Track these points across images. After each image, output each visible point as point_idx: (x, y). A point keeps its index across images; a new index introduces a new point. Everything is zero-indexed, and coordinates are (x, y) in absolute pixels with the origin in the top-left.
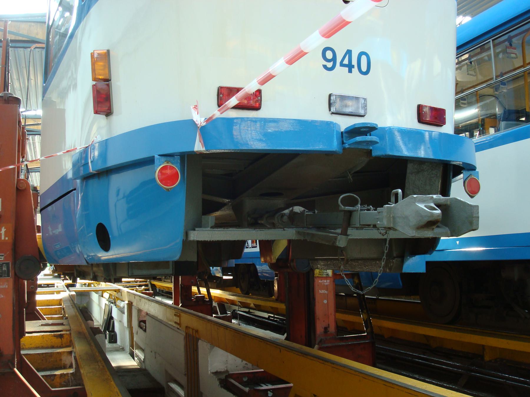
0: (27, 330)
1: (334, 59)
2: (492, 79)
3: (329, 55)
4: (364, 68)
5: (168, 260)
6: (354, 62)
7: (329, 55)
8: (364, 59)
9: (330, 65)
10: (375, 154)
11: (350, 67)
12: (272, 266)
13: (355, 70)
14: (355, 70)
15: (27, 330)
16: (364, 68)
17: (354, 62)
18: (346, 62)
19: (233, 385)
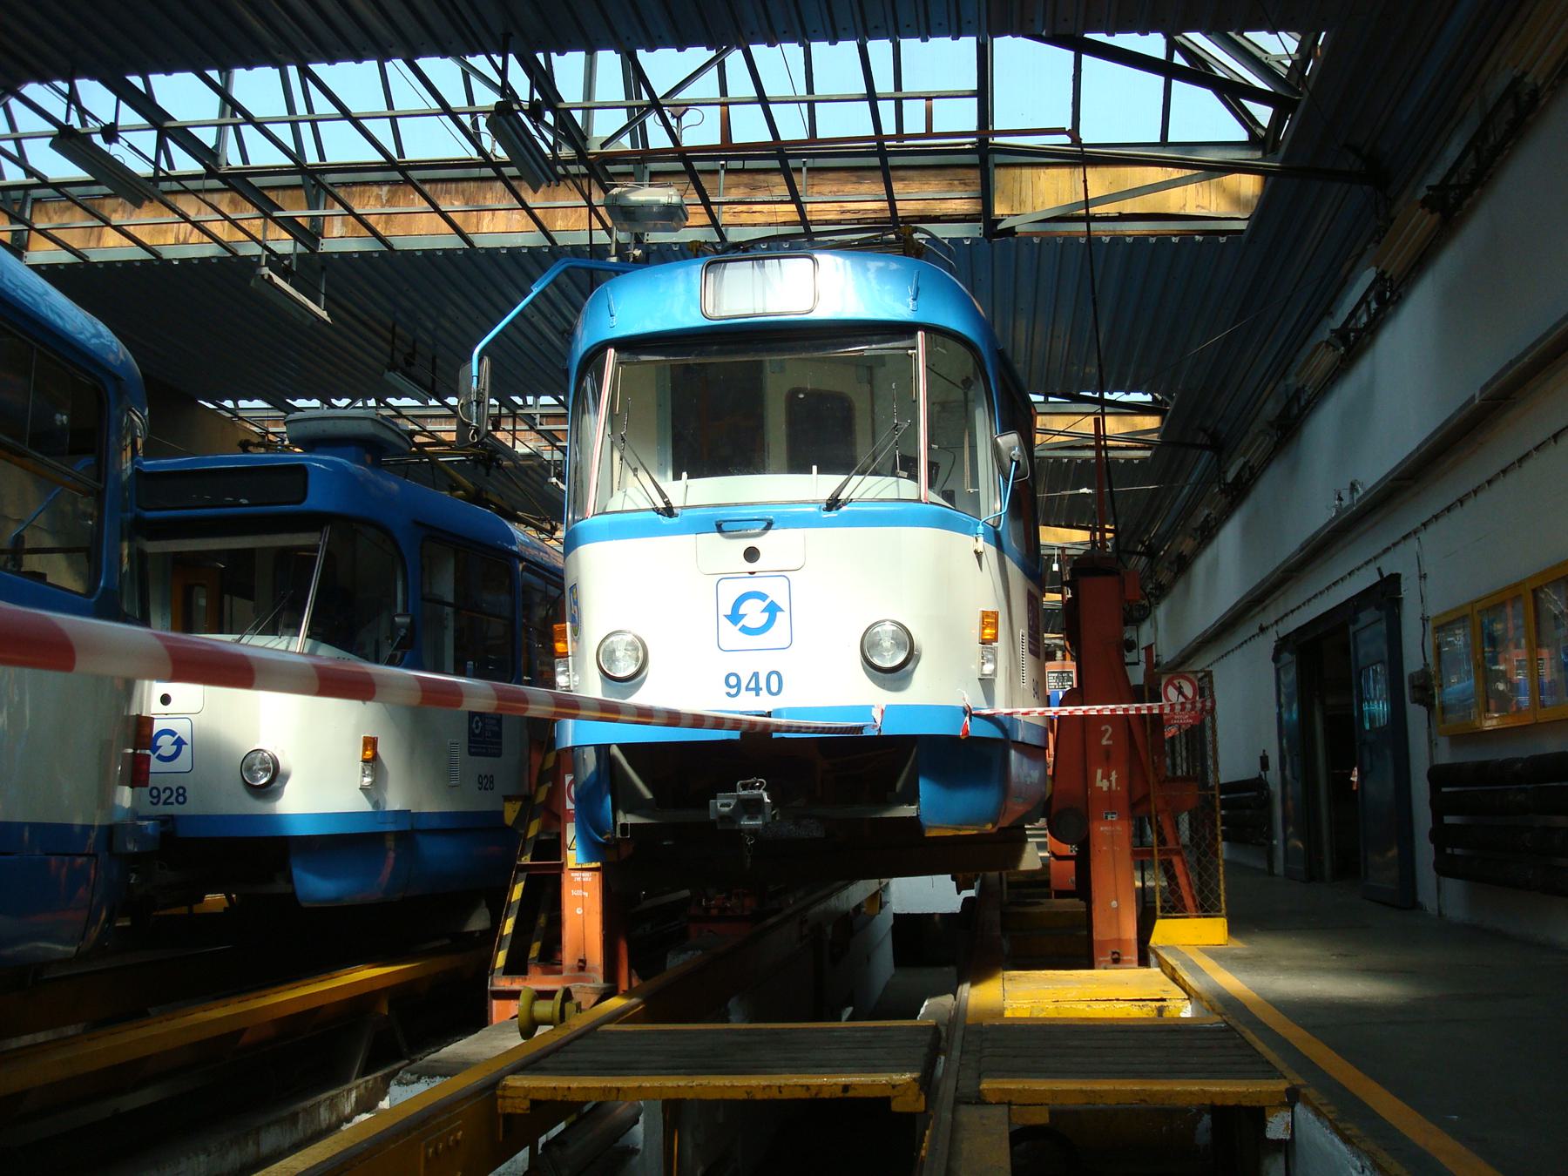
0: (1072, 863)
1: (738, 685)
2: (809, 170)
3: (733, 681)
4: (774, 688)
5: (582, 316)
6: (763, 684)
7: (733, 681)
8: (774, 678)
9: (733, 691)
10: (1008, 1014)
11: (757, 690)
12: (138, 473)
13: (764, 692)
14: (764, 692)
15: (1072, 863)
16: (774, 688)
17: (763, 684)
18: (752, 685)
19: (1344, 284)
